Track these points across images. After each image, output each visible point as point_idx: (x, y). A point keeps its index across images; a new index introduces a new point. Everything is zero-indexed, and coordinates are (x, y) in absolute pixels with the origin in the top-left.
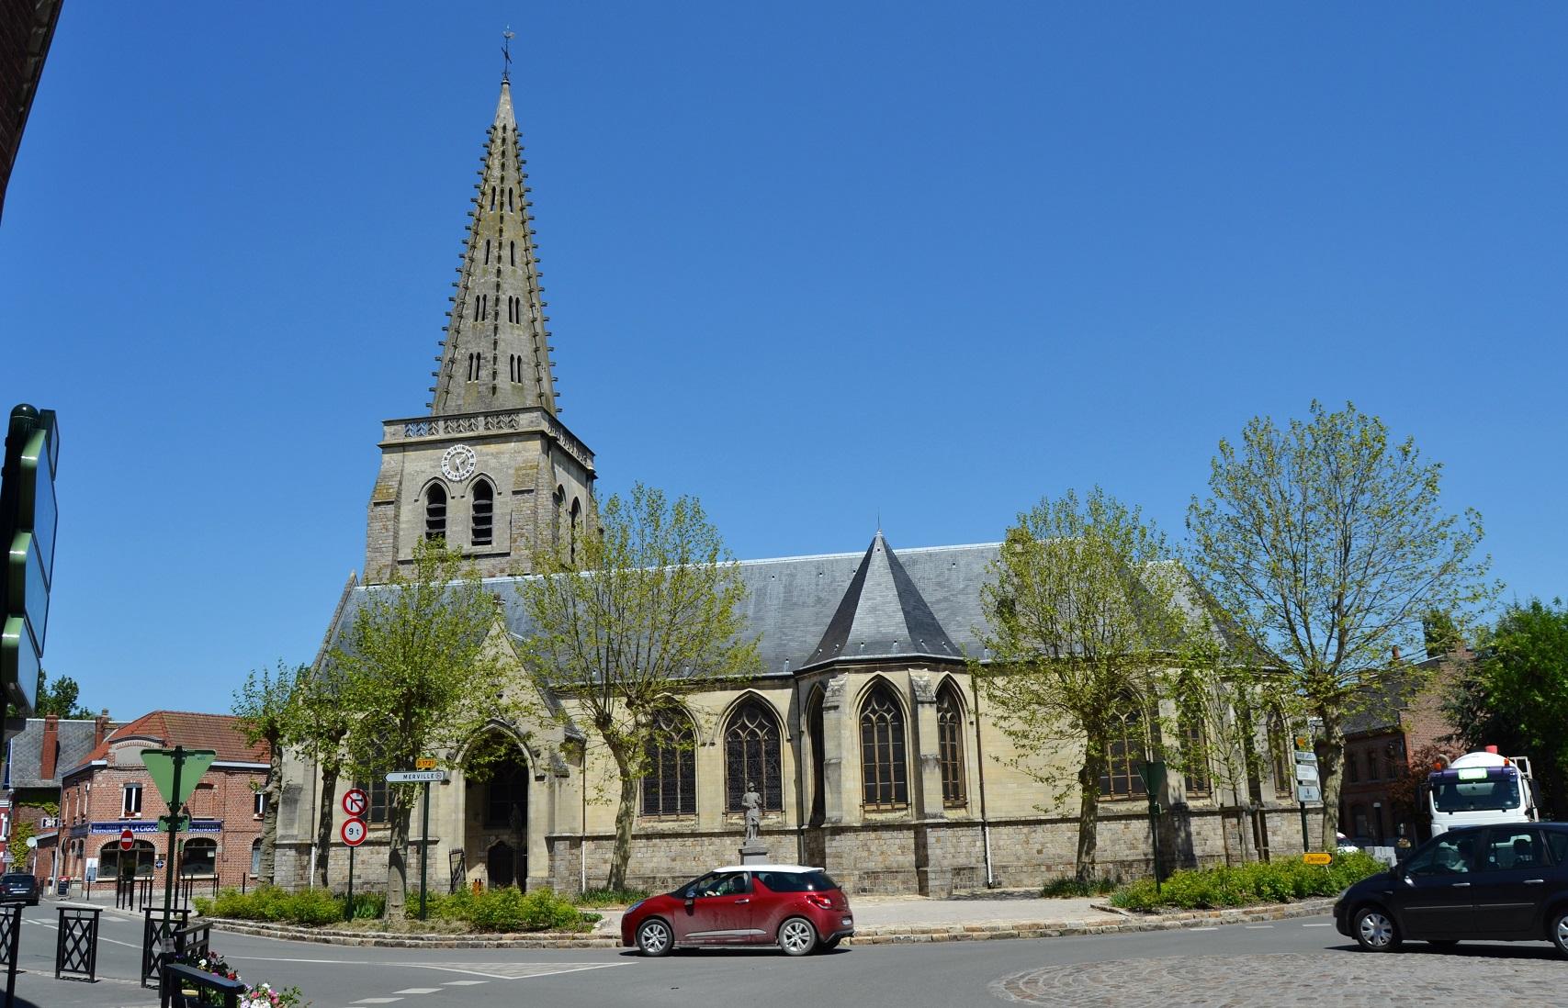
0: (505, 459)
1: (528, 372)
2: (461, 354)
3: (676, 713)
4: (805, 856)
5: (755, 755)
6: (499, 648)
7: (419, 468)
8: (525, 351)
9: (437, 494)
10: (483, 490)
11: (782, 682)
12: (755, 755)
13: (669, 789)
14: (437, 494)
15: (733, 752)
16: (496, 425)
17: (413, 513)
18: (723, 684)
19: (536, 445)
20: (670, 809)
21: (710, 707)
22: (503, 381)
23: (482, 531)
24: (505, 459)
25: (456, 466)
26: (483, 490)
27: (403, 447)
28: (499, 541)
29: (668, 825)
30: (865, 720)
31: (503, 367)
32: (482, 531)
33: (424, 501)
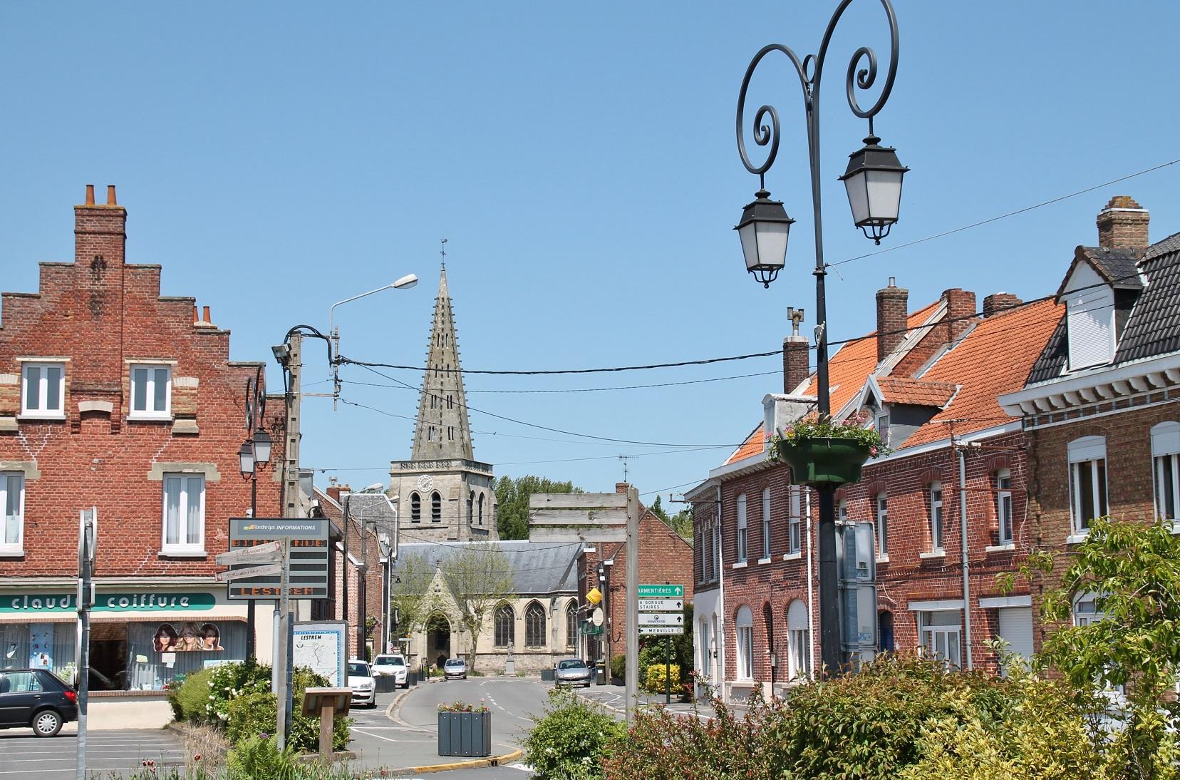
0: (446, 482)
1: (457, 434)
2: (425, 426)
3: (509, 608)
4: (103, 636)
5: (537, 624)
6: (438, 581)
7: (409, 485)
8: (455, 423)
9: (416, 497)
10: (436, 496)
11: (547, 596)
12: (537, 624)
13: (505, 636)
14: (416, 497)
15: (529, 622)
16: (440, 465)
17: (406, 505)
18: (522, 596)
19: (459, 477)
20: (537, 644)
21: (520, 606)
22: (445, 441)
23: (436, 515)
24: (446, 482)
25: (425, 485)
26: (436, 496)
27: (400, 475)
28: (444, 521)
29: (504, 650)
30: (568, 614)
31: (445, 434)
32: (436, 515)
33: (410, 500)
